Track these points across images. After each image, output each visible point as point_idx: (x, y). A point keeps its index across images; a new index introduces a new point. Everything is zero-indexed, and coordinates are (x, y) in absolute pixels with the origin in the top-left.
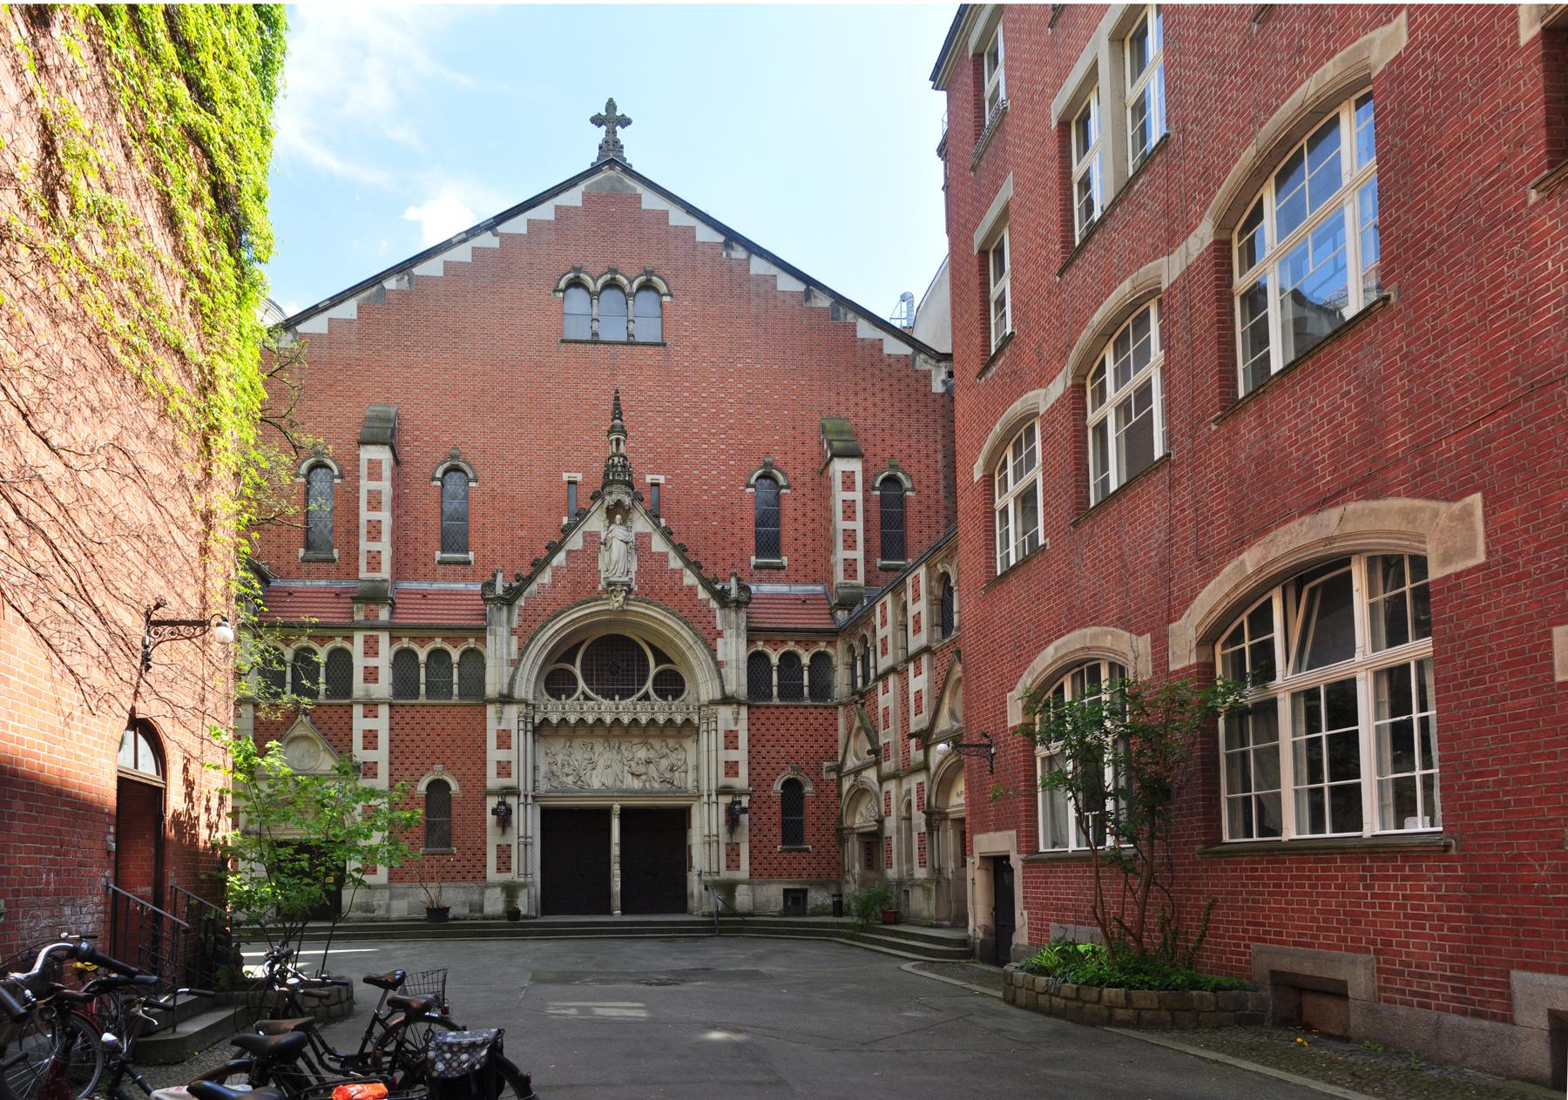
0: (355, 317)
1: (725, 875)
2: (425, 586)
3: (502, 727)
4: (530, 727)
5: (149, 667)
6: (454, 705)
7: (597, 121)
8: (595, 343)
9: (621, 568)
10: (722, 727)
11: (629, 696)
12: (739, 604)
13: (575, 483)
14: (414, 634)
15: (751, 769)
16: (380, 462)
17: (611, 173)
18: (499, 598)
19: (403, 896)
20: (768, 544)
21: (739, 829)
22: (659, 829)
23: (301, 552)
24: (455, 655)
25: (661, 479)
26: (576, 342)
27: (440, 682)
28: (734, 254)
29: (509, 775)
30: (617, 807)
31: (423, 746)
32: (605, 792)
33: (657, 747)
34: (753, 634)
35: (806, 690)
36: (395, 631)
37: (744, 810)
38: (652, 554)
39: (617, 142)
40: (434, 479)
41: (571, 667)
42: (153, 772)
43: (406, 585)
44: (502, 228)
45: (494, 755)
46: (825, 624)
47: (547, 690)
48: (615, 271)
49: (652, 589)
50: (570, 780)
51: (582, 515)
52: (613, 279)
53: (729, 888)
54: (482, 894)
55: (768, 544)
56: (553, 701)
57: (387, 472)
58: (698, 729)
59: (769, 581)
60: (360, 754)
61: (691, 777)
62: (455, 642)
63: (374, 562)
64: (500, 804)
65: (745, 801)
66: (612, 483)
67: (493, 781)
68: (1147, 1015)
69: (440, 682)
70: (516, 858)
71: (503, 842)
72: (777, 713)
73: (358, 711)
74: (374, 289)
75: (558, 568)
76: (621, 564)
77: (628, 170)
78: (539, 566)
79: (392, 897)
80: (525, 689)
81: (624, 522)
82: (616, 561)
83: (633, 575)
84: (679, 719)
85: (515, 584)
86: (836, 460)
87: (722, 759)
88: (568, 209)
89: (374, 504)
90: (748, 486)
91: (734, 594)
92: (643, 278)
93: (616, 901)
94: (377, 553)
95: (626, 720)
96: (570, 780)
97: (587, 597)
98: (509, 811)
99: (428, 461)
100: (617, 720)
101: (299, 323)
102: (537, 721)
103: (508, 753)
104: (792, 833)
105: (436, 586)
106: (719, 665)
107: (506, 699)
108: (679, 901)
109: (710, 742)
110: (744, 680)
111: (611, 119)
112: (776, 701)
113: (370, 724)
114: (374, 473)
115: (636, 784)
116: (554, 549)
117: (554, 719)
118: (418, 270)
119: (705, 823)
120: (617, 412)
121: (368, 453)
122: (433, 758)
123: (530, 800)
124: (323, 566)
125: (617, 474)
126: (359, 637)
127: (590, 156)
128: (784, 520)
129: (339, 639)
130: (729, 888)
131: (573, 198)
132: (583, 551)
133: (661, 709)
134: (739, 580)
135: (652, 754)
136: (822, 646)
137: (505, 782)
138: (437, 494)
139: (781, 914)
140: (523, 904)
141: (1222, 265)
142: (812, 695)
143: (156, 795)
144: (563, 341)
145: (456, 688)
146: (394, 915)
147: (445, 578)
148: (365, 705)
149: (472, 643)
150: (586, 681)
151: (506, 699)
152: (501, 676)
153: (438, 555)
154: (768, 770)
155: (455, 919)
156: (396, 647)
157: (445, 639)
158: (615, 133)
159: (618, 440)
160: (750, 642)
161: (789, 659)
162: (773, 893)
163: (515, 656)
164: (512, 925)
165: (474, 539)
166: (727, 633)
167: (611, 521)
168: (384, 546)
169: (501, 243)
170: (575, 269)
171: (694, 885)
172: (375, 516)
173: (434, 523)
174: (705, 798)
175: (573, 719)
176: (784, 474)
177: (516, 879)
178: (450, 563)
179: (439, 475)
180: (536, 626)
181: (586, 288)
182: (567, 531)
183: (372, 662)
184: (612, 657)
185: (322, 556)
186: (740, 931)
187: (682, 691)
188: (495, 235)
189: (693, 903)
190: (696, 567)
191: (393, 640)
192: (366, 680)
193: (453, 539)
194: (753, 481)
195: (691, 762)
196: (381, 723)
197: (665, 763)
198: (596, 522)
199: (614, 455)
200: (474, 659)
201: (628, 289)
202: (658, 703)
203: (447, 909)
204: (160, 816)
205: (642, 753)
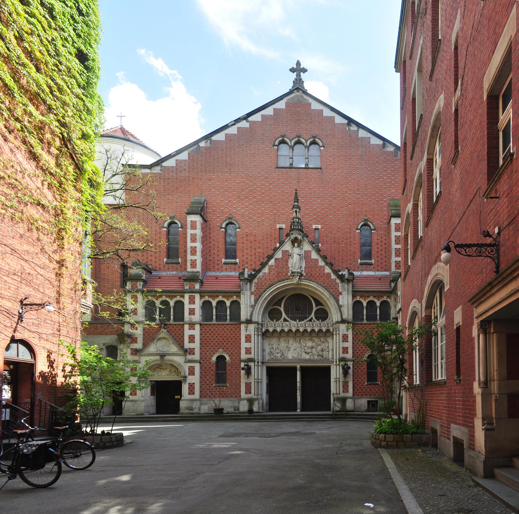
0: (187, 159)
1: (342, 395)
2: (218, 274)
3: (247, 333)
5: (22, 321)
6: (227, 325)
7: (292, 70)
8: (291, 168)
9: (297, 266)
11: (303, 320)
12: (348, 281)
13: (282, 229)
14: (210, 294)
16: (196, 222)
17: (298, 93)
18: (246, 279)
19: (206, 404)
21: (348, 376)
23: (165, 260)
24: (228, 303)
25: (319, 227)
26: (283, 168)
27: (222, 315)
28: (351, 128)
29: (250, 353)
30: (298, 366)
31: (214, 341)
32: (294, 360)
33: (316, 341)
35: (378, 317)
36: (202, 294)
38: (311, 260)
39: (301, 80)
40: (221, 228)
41: (279, 308)
42: (30, 358)
43: (210, 273)
44: (250, 119)
45: (244, 345)
46: (387, 289)
48: (299, 137)
49: (311, 274)
51: (282, 243)
52: (298, 140)
53: (343, 401)
54: (239, 403)
57: (199, 226)
59: (366, 270)
60: (187, 345)
61: (331, 353)
62: (228, 298)
63: (194, 264)
65: (350, 364)
67: (244, 356)
68: (390, 443)
69: (222, 315)
70: (254, 388)
71: (248, 381)
72: (365, 326)
73: (186, 327)
74: (195, 147)
75: (271, 266)
77: (305, 92)
79: (201, 404)
80: (257, 317)
81: (299, 246)
82: (295, 263)
83: (303, 269)
84: (324, 329)
86: (392, 218)
87: (341, 346)
88: (279, 110)
89: (194, 240)
90: (357, 229)
91: (346, 276)
92: (312, 139)
93: (299, 406)
94: (195, 260)
95: (301, 330)
96: (279, 355)
97: (284, 278)
99: (218, 221)
101: (163, 162)
102: (263, 330)
103: (249, 344)
104: (372, 377)
105: (223, 274)
106: (340, 307)
107: (249, 322)
108: (328, 407)
109: (337, 338)
110: (351, 313)
111: (298, 70)
112: (365, 322)
113: (192, 332)
114: (194, 227)
115: (307, 357)
116: (270, 258)
117: (271, 330)
118: (214, 138)
119: (336, 372)
120: (296, 200)
121: (191, 218)
122: (219, 347)
123: (260, 364)
124: (175, 265)
125: (297, 226)
126: (187, 296)
127: (289, 86)
129: (178, 297)
130: (343, 401)
131: (281, 105)
132: (282, 259)
133: (317, 325)
134: (349, 270)
135: (314, 344)
136: (385, 298)
137: (249, 356)
138: (223, 235)
139: (366, 411)
140: (255, 409)
141: (430, 168)
142: (381, 319)
143: (31, 367)
144: (277, 168)
145: (228, 317)
146: (202, 412)
147: (226, 270)
148: (189, 324)
149: (235, 298)
151: (249, 322)
152: (247, 312)
153: (224, 260)
154: (362, 351)
155: (228, 413)
156: (203, 300)
157: (223, 296)
158: (300, 76)
159: (296, 212)
160: (354, 296)
161: (371, 304)
162: (363, 402)
163: (253, 303)
164: (250, 415)
165: (239, 254)
167: (294, 246)
168: (198, 258)
169: (250, 125)
170: (282, 136)
172: (194, 245)
173: (222, 247)
174: (335, 363)
175: (279, 330)
177: (254, 397)
178: (228, 264)
179: (224, 226)
180: (262, 291)
181: (288, 144)
182: (276, 250)
183: (192, 306)
184: (297, 303)
185: (174, 261)
186: (345, 418)
187: (327, 317)
188: (247, 122)
190: (331, 265)
191: (201, 297)
192: (190, 314)
193: (230, 253)
195: (331, 348)
196: (196, 332)
197: (319, 348)
198: (287, 246)
199: (294, 218)
200: (236, 305)
201: (305, 145)
203: (223, 409)
204: (33, 374)
205: (310, 344)
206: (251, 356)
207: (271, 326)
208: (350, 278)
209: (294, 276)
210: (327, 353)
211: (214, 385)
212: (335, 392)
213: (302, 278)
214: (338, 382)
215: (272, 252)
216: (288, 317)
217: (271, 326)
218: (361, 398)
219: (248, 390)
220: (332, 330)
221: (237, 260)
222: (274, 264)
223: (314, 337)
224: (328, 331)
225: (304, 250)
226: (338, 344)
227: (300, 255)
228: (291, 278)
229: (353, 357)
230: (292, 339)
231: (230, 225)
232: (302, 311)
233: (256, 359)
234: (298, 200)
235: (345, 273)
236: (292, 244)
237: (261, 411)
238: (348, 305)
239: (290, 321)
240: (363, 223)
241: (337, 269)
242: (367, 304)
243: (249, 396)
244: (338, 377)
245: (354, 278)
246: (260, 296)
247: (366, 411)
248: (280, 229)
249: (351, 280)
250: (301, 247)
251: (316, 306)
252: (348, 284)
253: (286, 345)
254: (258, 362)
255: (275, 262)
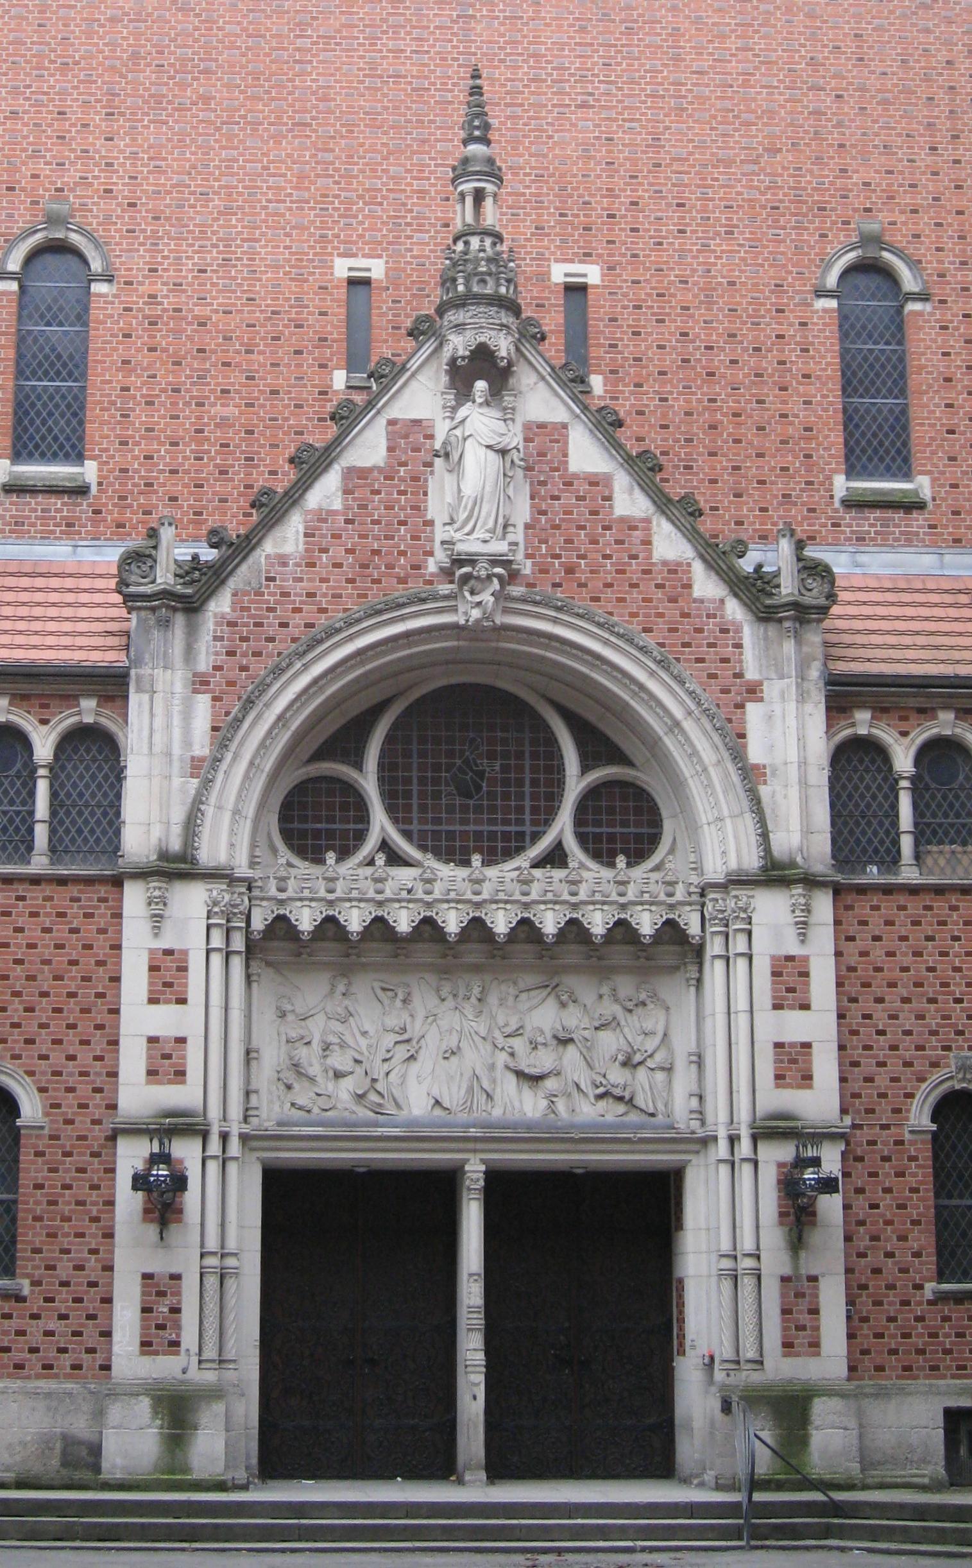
1: (781, 1369)
4: (238, 943)
6: (36, 880)
10: (765, 947)
12: (805, 614)
13: (366, 282)
15: (848, 1066)
20: (878, 440)
21: (815, 1237)
22: (597, 1231)
29: (180, 1075)
30: (475, 1170)
34: (843, 694)
37: (828, 1185)
45: (140, 1019)
47: (288, 835)
49: (570, 570)
50: (346, 1087)
51: (386, 377)
53: (790, 1409)
54: (99, 1414)
55: (878, 440)
56: (303, 868)
58: (699, 951)
59: (883, 540)
61: (683, 1081)
64: (155, 1159)
65: (831, 1160)
66: (461, 302)
67: (137, 1095)
71: (159, 1265)
75: (323, 516)
76: (487, 509)
78: (271, 509)
80: (225, 841)
83: (518, 535)
85: (209, 554)
90: (820, 293)
91: (788, 587)
93: (472, 1439)
96: (346, 1087)
97: (399, 592)
98: (179, 1182)
100: (477, 922)
107: (177, 867)
115: (530, 1105)
116: (310, 464)
119: (722, 1222)
120: (478, 129)
123: (234, 1148)
125: (478, 279)
128: (914, 380)
130: (790, 1409)
133: (594, 892)
135: (573, 1019)
145: (41, 833)
149: (88, 710)
150: (391, 810)
151: (177, 867)
154: (895, 1066)
163: (202, 746)
165: (99, 427)
166: (771, 690)
171: (694, 1398)
174: (722, 1149)
176: (914, 264)
179: (14, 264)
180: (260, 668)
182: (346, 418)
184: (471, 740)
186: (827, 1532)
187: (654, 840)
189: (689, 1449)
190: (685, 512)
194: (832, 280)
195: (683, 1043)
197: (609, 1042)
198: (421, 397)
200: (95, 753)
202: (592, 875)
205: (545, 1016)
206: (181, 1097)
207: (311, 892)
208: (808, 600)
209: (466, 578)
210: (660, 1076)
211: (930, 1286)
212: (728, 1352)
213: (517, 590)
214: (747, 1283)
215: (333, 430)
216: (407, 835)
217: (311, 892)
218: (902, 1391)
219: (159, 1335)
220: (694, 929)
221: (90, 471)
222: (337, 505)
223: (576, 969)
224: (671, 931)
225: (520, 420)
226: (742, 1021)
227: (503, 452)
228: (445, 588)
229: (844, 1111)
230: (432, 978)
231: (49, 260)
232: (491, 795)
233: (214, 1113)
234: (486, 127)
235: (778, 557)
236: (453, 384)
237: (241, 1476)
238: (803, 763)
239: (430, 861)
240: (852, 255)
241: (728, 535)
242: (918, 761)
243: (165, 1367)
244: (748, 1245)
245: (832, 597)
246: (249, 703)
247: (934, 1487)
248: (352, 282)
249: (795, 609)
250: (508, 399)
251: (585, 769)
252: (799, 642)
253: (392, 1021)
254: (224, 1137)
255: (347, 492)
